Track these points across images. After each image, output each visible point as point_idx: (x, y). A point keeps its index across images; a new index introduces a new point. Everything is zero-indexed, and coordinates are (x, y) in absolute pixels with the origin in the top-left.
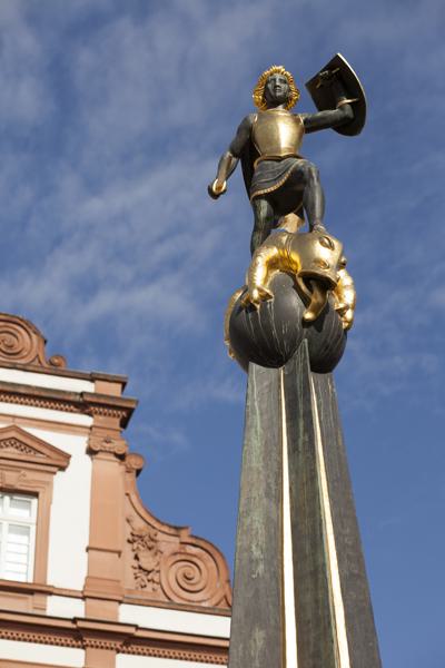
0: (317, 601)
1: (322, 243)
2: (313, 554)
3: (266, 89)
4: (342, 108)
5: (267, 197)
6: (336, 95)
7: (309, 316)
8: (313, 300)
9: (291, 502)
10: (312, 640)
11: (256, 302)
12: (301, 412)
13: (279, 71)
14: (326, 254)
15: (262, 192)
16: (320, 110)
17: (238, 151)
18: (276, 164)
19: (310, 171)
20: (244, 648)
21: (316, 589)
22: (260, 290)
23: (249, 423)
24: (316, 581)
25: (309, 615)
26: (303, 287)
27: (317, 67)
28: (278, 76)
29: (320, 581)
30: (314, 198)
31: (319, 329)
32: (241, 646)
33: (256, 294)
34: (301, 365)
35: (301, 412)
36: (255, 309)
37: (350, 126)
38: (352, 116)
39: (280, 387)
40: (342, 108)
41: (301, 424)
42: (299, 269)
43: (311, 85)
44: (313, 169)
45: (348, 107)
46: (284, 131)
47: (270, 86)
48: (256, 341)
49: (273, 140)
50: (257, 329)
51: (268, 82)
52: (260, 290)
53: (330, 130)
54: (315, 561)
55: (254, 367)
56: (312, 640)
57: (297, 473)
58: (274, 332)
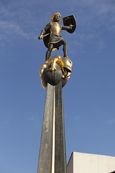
0: (60, 141)
1: (69, 61)
2: (60, 131)
3: (55, 17)
4: (70, 27)
5: (53, 44)
6: (69, 23)
7: (63, 77)
8: (65, 74)
9: (55, 119)
10: (59, 149)
11: (53, 71)
12: (59, 98)
13: (58, 14)
14: (69, 64)
15: (52, 43)
16: (64, 25)
17: (46, 30)
18: (56, 37)
19: (66, 42)
20: (43, 147)
21: (61, 138)
22: (54, 68)
23: (47, 97)
24: (61, 137)
25: (58, 143)
26: (63, 70)
27: (67, 15)
28: (58, 15)
29: (62, 137)
30: (66, 49)
31: (64, 80)
32: (43, 147)
33: (53, 69)
34: (60, 87)
35: (59, 98)
36: (52, 72)
37: (71, 31)
38: (72, 29)
39: (54, 90)
40: (70, 27)
41: (59, 100)
42: (63, 66)
43: (64, 19)
44: (66, 42)
45: (72, 27)
46: (58, 28)
47: (56, 17)
48: (49, 78)
49: (55, 31)
50: (51, 76)
51: (56, 16)
52: (54, 68)
53: (66, 31)
54: (61, 132)
55: (49, 84)
56: (59, 149)
57: (57, 111)
58: (55, 78)
